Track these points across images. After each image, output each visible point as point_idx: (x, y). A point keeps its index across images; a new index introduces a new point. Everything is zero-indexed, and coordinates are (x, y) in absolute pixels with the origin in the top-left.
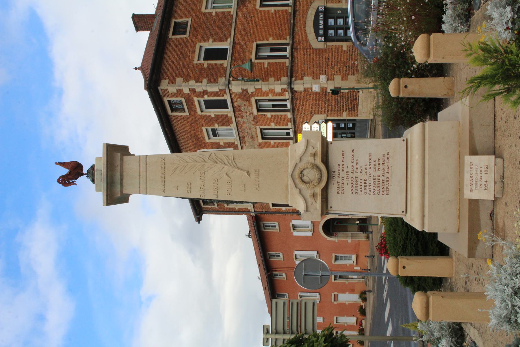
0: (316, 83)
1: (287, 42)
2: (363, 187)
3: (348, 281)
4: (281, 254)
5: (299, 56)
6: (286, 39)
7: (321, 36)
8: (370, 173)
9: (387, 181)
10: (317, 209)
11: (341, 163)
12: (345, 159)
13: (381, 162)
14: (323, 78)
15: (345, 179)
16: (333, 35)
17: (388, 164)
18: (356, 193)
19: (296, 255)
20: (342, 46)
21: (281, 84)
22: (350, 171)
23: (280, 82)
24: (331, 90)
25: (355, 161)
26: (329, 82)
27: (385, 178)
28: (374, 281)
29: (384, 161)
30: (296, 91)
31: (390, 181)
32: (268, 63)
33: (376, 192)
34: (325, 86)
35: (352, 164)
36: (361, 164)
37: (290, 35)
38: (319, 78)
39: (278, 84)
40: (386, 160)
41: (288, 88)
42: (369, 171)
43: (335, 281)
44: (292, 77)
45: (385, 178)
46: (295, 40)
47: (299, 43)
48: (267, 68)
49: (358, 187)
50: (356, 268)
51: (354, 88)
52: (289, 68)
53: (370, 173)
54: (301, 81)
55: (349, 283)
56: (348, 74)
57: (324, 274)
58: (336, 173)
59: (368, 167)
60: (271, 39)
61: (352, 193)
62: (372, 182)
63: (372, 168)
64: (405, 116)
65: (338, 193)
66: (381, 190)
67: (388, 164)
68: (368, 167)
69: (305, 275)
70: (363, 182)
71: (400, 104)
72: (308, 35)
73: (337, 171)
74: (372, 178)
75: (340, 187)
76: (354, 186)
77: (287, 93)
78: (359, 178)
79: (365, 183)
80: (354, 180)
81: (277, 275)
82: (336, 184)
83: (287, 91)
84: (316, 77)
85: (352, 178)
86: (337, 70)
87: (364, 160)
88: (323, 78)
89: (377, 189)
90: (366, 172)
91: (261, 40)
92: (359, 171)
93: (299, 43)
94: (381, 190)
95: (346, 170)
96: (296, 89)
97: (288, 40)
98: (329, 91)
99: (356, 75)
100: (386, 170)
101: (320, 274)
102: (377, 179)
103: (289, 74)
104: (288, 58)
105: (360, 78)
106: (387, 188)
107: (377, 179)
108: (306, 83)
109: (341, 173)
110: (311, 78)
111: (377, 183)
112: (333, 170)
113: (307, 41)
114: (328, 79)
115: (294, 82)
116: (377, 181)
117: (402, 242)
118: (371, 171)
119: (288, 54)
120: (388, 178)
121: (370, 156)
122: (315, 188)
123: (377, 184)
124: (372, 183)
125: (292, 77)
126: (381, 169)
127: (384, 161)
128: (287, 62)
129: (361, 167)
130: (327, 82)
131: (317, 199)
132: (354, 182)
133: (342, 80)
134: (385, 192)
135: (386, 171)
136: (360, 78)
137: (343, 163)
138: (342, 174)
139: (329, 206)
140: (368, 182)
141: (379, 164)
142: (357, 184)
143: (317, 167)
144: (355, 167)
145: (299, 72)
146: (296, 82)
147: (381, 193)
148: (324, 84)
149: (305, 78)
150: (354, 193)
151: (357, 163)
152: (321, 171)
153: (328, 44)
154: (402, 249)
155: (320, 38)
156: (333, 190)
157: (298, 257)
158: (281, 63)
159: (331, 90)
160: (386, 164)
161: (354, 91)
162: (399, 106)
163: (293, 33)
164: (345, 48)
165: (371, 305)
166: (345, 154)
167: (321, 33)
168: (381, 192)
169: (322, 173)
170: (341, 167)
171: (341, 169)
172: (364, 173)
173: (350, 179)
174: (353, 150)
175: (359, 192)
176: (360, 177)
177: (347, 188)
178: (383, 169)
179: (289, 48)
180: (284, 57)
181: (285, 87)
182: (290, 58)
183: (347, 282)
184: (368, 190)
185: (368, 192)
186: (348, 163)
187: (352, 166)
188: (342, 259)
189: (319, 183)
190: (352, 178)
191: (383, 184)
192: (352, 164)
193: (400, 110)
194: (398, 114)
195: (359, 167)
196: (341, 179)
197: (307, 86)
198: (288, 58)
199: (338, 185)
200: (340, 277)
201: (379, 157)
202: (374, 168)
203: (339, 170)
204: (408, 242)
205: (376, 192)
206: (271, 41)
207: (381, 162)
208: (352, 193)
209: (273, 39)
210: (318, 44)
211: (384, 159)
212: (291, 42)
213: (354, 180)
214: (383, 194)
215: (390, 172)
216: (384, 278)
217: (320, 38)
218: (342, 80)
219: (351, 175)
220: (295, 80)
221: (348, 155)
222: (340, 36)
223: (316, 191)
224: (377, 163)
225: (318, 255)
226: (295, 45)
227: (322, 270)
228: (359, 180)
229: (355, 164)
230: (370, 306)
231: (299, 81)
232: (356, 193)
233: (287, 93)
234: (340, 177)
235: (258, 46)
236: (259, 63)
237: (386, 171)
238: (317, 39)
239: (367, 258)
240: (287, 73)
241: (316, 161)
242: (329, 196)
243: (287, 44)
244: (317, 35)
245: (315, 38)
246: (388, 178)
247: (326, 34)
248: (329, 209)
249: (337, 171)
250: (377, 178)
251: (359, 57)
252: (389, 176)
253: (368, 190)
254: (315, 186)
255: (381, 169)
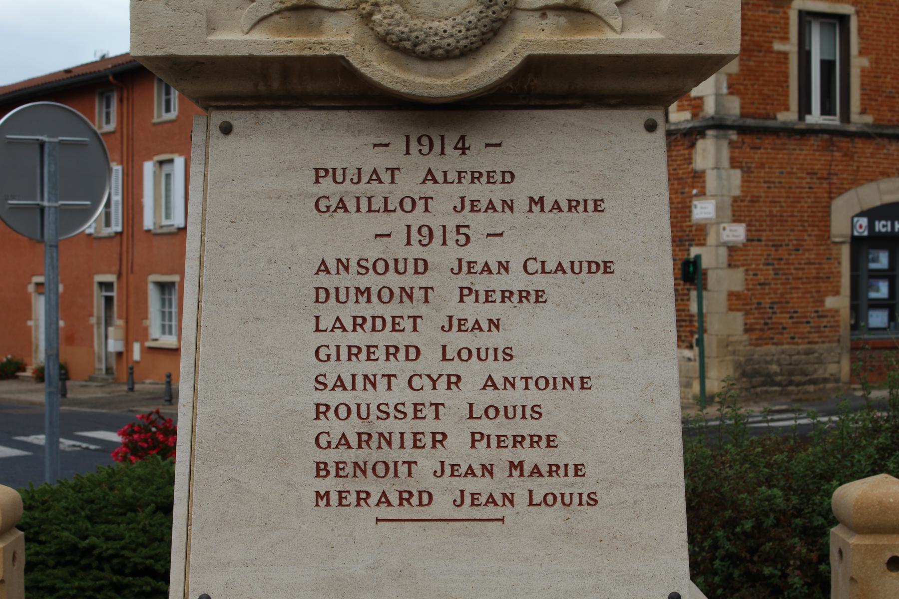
0: (718, 208)
1: (855, 117)
2: (361, 338)
3: (99, 324)
4: (173, 115)
5: (807, 154)
6: (863, 112)
7: (871, 226)
8: (454, 381)
9: (405, 498)
10: (211, 28)
11: (519, 192)
12: (548, 218)
13: (530, 456)
14: (737, 233)
15: (417, 218)
16: (873, 266)
17: (521, 498)
18: (321, 295)
19: (171, 161)
20: (837, 293)
21: (718, 96)
22: (468, 253)
23: (725, 91)
24: (698, 257)
25: (539, 282)
26: (724, 251)
27: (424, 475)
28: (94, 403)
29: (536, 471)
30: (693, 145)
31: (406, 512)
32: (786, 55)
33: (335, 427)
34: (711, 240)
35: (516, 266)
36: (520, 326)
37: (875, 125)
38: (736, 220)
39: (717, 87)
40: (542, 486)
41: (705, 119)
42: (473, 373)
43: (96, 287)
44: (742, 130)
45: (424, 475)
46: (859, 143)
47: (849, 155)
48: (770, 51)
49: (364, 303)
50: (137, 347)
51: (702, 330)
52: (770, 123)
53: (454, 381)
54: (726, 163)
55: (92, 326)
56: (747, 313)
57: (49, 217)
58: (453, 161)
59: (499, 370)
60: (865, 62)
61: (323, 268)
62: (401, 394)
63: (490, 397)
64: (715, 546)
65: (319, 174)
66: (349, 455)
67: (521, 498)
68: (499, 370)
69: (42, 145)
70: (399, 339)
71: (777, 524)
72: (873, 185)
73: (468, 163)
74: (428, 396)
75: (363, 188)
76: (370, 281)
77: (687, 115)
78: (423, 310)
79: (391, 352)
80: (410, 280)
81: (108, 106)
82: (381, 160)
83: (695, 116)
84: (739, 210)
85: (422, 266)
86: (761, 278)
87: (540, 339)
88: (737, 233)
89: (352, 427)
90: (466, 354)
91: (860, 29)
92: (472, 310)
93: (849, 155)
94: (349, 455)
95: (479, 223)
96: (700, 144)
97: (859, 119)
98: (694, 251)
99: (745, 337)
100: (481, 485)
101: (46, 203)
102: (419, 426)
103: (750, 122)
104: (801, 118)
105: (734, 353)
106: (362, 498)
107: (419, 426)
108: (719, 177)
109: (456, 190)
110: (737, 192)
111: (393, 426)
112: (475, 142)
113: (856, 182)
114: (732, 249)
115: (725, 137)
116: (408, 426)
117: (109, 548)
118: (471, 390)
119: (815, 118)
120: (427, 498)
121: (568, 382)
122: (348, 19)
123: (384, 427)
124: (392, 398)
125: (742, 130)
126: (483, 454)
127: (536, 471)
128: (788, 116)
129: (495, 324)
130: (724, 244)
131: (279, 31)
132: (393, 280)
133: (731, 295)
134: (330, 484)
135: (471, 485)
136: (734, 353)
137: (522, 204)
138: (445, 197)
139: (237, 119)
140: (400, 367)
141: (518, 440)
142: (387, 295)
143: (490, 33)
144: (498, 282)
145: (757, 156)
146: (725, 144)
147: (322, 456)
148: (718, 234)
149: (737, 174)
150: (324, 280)
151: (524, 296)
152: (466, 52)
153: (846, 251)
154: (74, 548)
155: (864, 221)
156: (345, 142)
157: (166, 168)
158: (786, 95)
159: (698, 257)
160: (519, 487)
161: (692, 333)
162: (769, 521)
163: (882, 136)
164: (830, 302)
165: (23, 397)
166: (578, 217)
167: (881, 226)
168: (330, 457)
169: (454, 66)
170: (498, 192)
171: (480, 191)
172: (457, 340)
173: (416, 251)
174: (607, 268)
175: (329, 313)
176: (433, 318)
177: (355, 235)
178: (488, 470)
179: (834, 121)
180: (805, 108)
181: (710, 108)
182: (801, 126)
183: (93, 320)
184: (346, 369)
185: (332, 371)
186: (521, 239)
187: (504, 267)
188: (163, 305)
189: (383, 39)
190: (422, 266)
191: (389, 469)
192: (516, 266)
193: (748, 525)
194: (728, 513)
195: (496, 310)
196: (418, 191)
197: (711, 182)
198: (801, 118)
199: (375, 176)
200: (109, 300)
201: (562, 436)
202: (492, 411)
203: (476, 177)
204: (109, 576)
205: (335, 427)
206: (859, 63)
207: (530, 456)
208: (323, 268)
209: (863, 70)
210: (846, 216)
211: (553, 470)
212: (852, 128)
213: (410, 280)
214: (321, 469)
215: (467, 511)
216: (40, 439)
217: (864, 221)
218: (731, 295)
219: (443, 256)
220: (731, 143)
221: (578, 238)
222: (870, 287)
223: (330, 21)
224: (526, 427)
225: (173, 229)
226: (843, 143)
227: (61, 210)
228: (407, 309)
229: (516, 281)
230: (20, 392)
231: (726, 153)
232: (321, 295)
233: (687, 115)
234: (429, 189)
235: (843, 19)
236: (787, 24)
237: (471, 485)
238: (861, 214)
239: (165, 379)
240: (753, 116)
241: (533, 20)
242: (300, 116)
243: (846, 116)
244: (873, 214)
245: (866, 207)
246: (427, 498)
247: (875, 241)
248: (218, 118)
249: (468, 163)
250: (428, 426)
251: (801, 347)
252: (442, 506)
253: (346, 369)
254: (367, 18)
255: (483, 454)
